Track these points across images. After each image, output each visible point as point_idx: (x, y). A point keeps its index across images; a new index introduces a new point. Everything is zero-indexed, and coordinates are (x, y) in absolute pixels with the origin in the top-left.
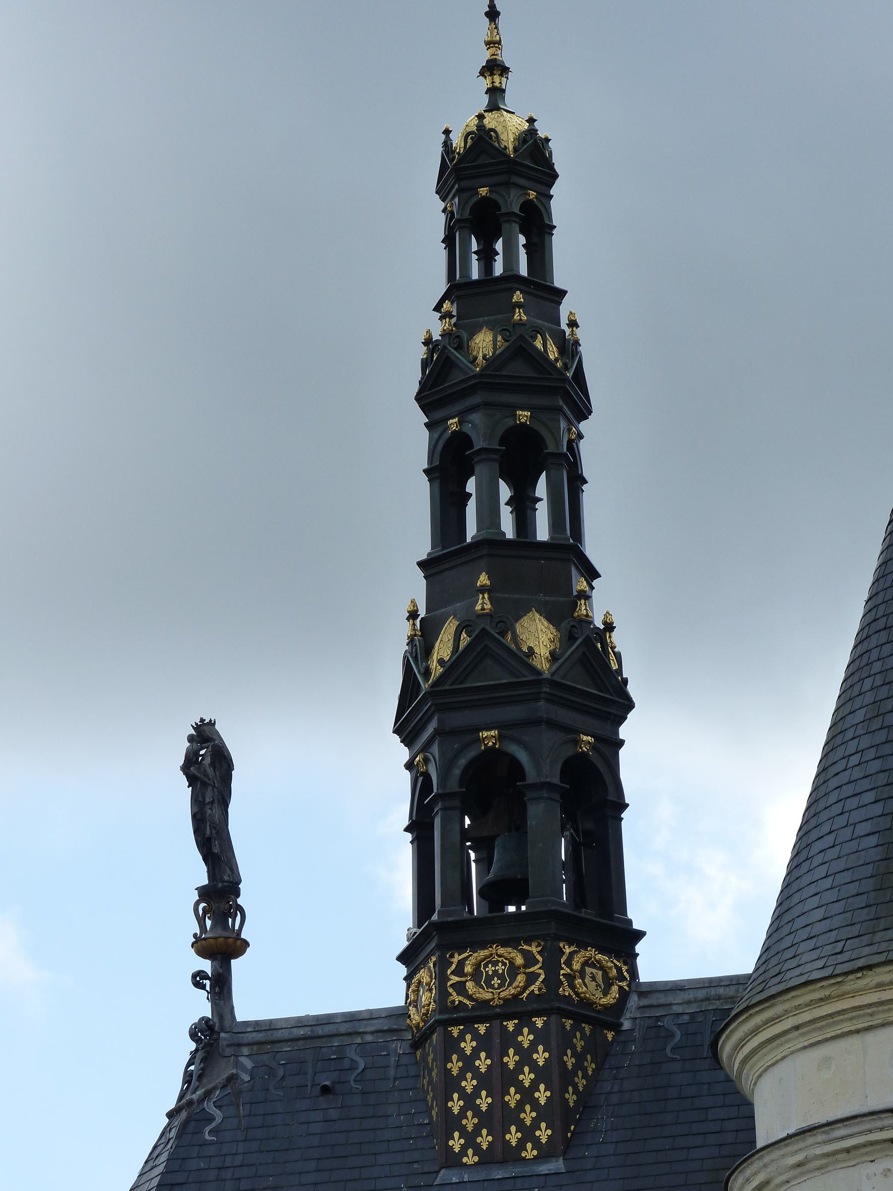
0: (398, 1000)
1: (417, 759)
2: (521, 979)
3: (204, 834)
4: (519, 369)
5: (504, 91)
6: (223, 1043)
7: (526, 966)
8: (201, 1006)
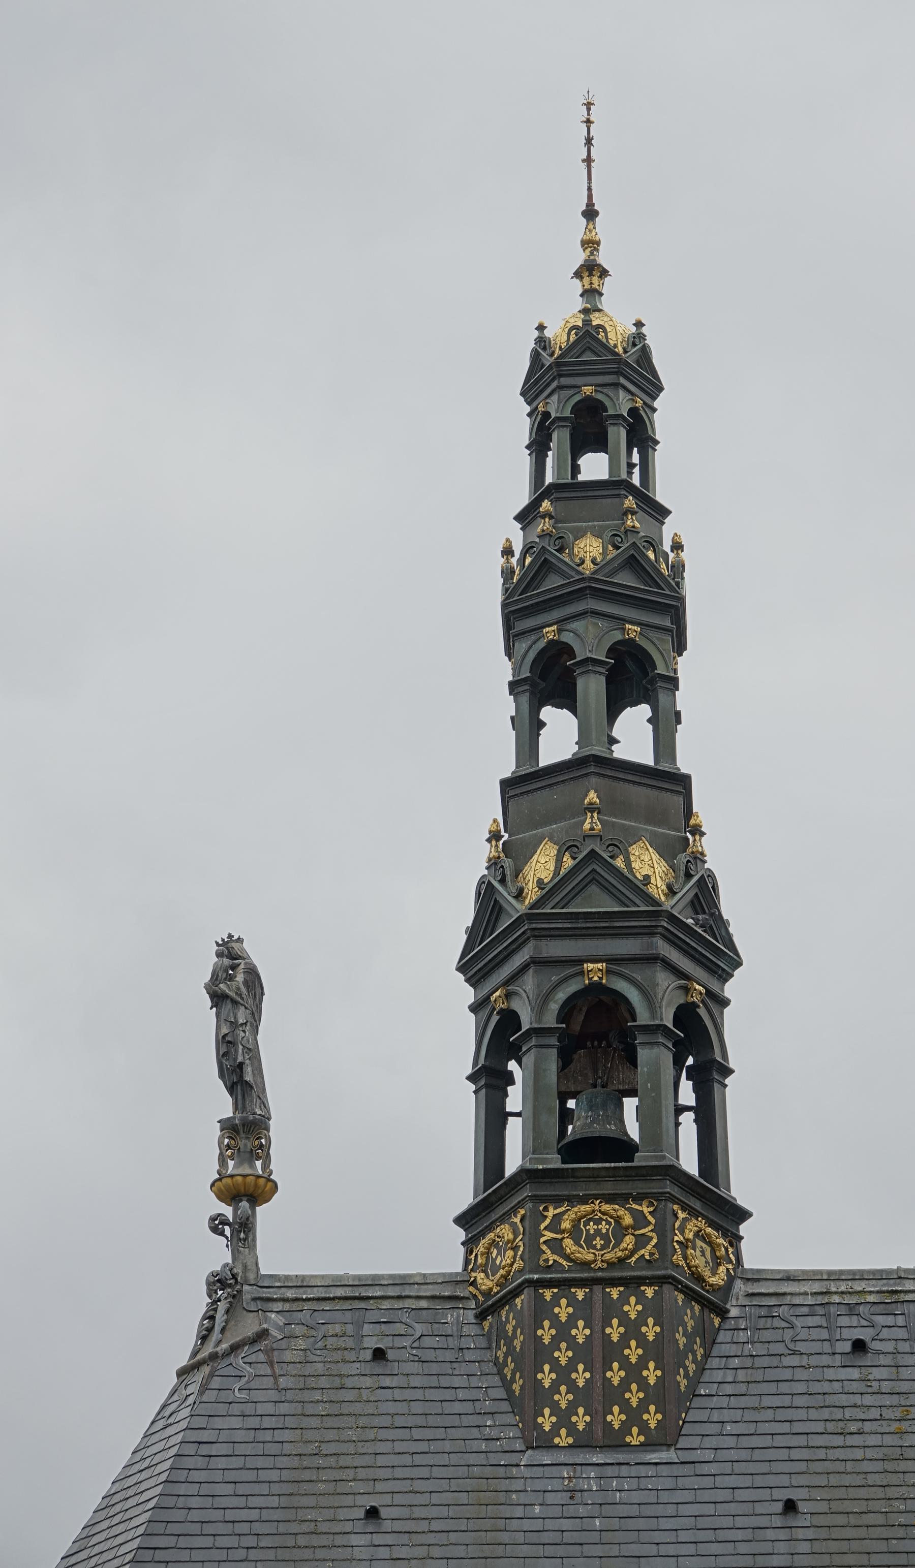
0: (455, 1265)
1: (498, 993)
2: (629, 1241)
3: (235, 1059)
4: (626, 579)
5: (601, 294)
6: (246, 1297)
7: (635, 1228)
8: (218, 1254)
